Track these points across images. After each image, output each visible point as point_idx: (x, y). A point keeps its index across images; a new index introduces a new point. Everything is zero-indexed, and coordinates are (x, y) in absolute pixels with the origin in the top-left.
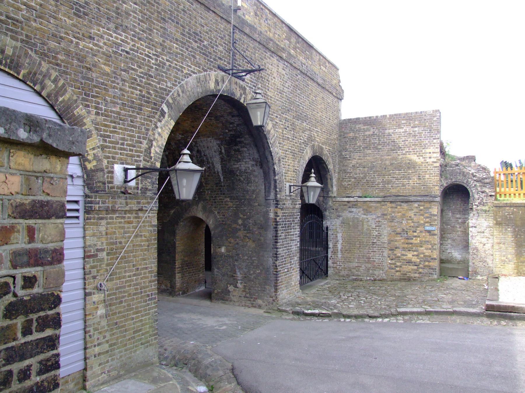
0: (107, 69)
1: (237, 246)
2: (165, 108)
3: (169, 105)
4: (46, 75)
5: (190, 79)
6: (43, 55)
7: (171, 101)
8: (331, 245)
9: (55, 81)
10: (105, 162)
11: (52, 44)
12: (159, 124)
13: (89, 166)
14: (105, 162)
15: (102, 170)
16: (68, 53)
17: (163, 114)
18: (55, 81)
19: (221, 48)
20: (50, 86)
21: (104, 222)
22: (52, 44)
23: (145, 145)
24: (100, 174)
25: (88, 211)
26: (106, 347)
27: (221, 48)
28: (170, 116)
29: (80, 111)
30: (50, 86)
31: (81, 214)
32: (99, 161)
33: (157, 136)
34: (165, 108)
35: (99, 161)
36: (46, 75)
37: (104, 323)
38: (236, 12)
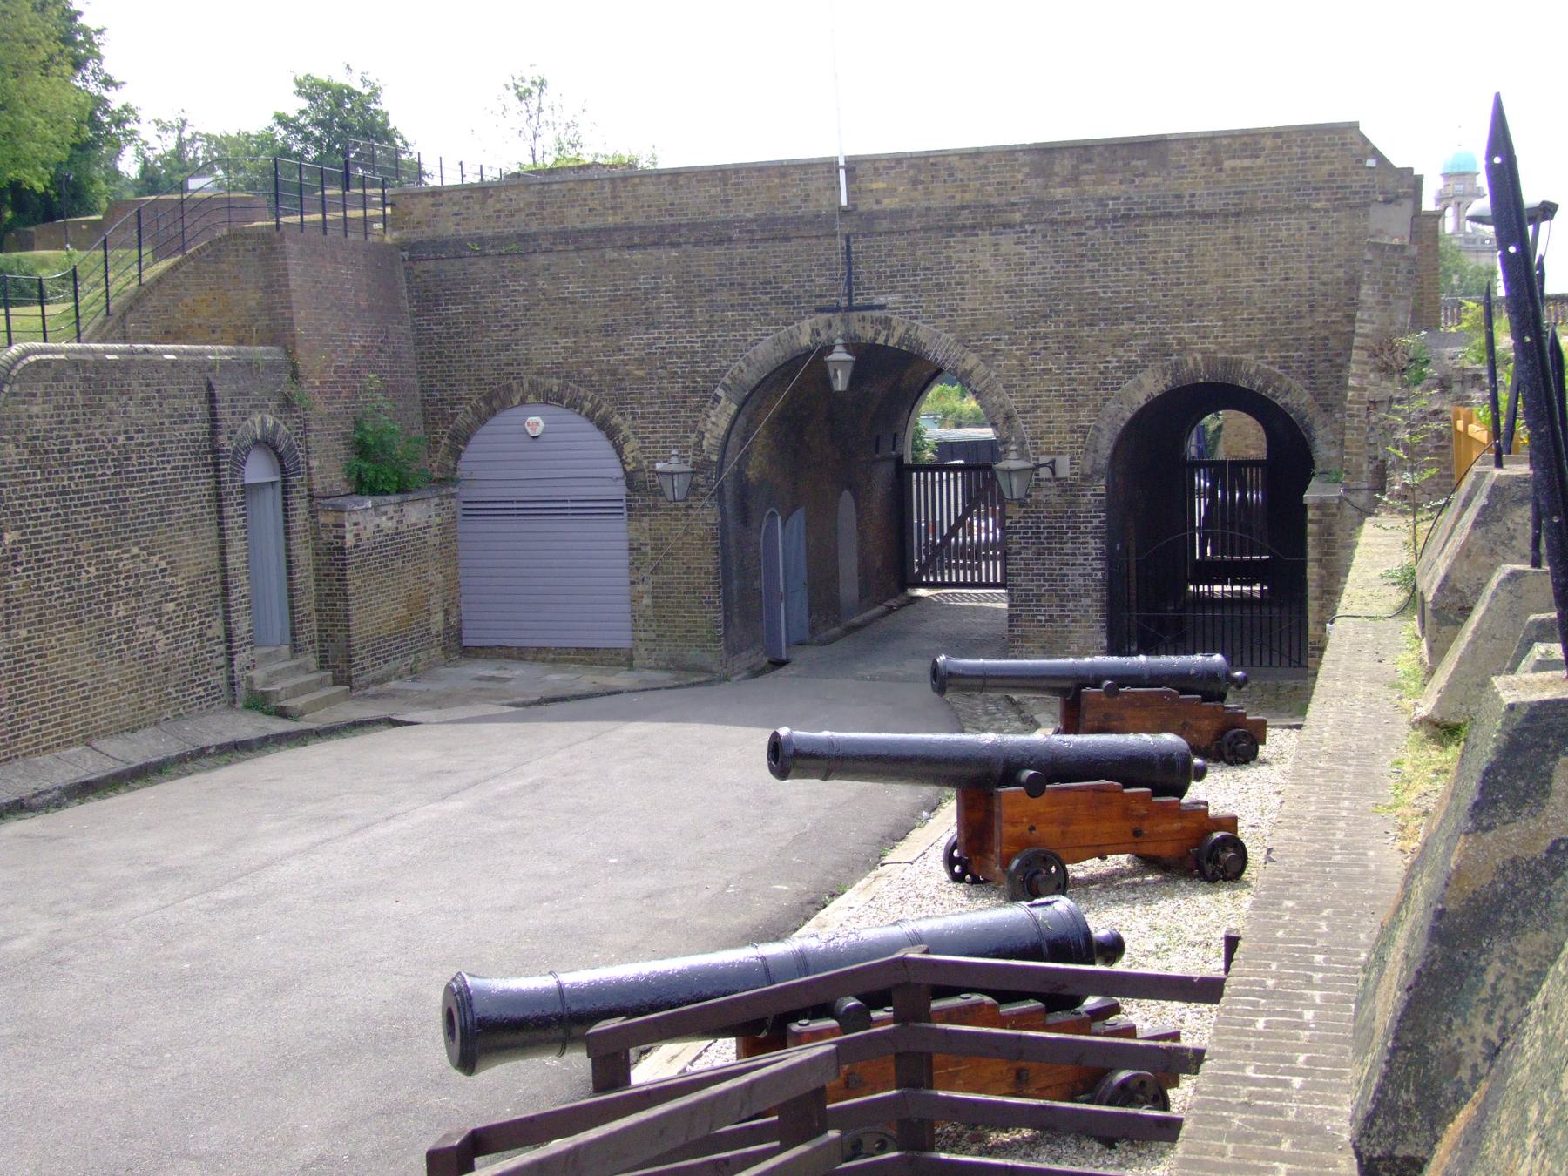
0: (641, 373)
1: (303, 976)
2: (720, 392)
3: (726, 388)
4: (585, 398)
5: (761, 346)
6: (580, 383)
7: (728, 382)
8: (77, 357)
9: (592, 400)
10: (646, 462)
11: (587, 370)
12: (712, 412)
13: (629, 468)
14: (646, 462)
15: (642, 470)
16: (601, 373)
17: (717, 399)
18: (592, 400)
19: (821, 281)
20: (588, 405)
21: (646, 519)
22: (587, 370)
23: (693, 438)
24: (640, 475)
25: (630, 508)
26: (653, 636)
27: (821, 281)
28: (728, 399)
29: (616, 420)
30: (588, 405)
31: (624, 510)
32: (639, 462)
33: (710, 426)
34: (720, 392)
35: (639, 462)
36: (585, 398)
37: (650, 612)
38: (989, 797)
